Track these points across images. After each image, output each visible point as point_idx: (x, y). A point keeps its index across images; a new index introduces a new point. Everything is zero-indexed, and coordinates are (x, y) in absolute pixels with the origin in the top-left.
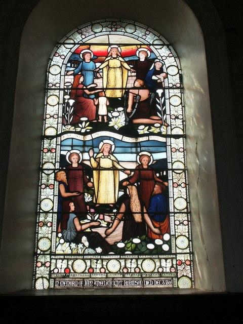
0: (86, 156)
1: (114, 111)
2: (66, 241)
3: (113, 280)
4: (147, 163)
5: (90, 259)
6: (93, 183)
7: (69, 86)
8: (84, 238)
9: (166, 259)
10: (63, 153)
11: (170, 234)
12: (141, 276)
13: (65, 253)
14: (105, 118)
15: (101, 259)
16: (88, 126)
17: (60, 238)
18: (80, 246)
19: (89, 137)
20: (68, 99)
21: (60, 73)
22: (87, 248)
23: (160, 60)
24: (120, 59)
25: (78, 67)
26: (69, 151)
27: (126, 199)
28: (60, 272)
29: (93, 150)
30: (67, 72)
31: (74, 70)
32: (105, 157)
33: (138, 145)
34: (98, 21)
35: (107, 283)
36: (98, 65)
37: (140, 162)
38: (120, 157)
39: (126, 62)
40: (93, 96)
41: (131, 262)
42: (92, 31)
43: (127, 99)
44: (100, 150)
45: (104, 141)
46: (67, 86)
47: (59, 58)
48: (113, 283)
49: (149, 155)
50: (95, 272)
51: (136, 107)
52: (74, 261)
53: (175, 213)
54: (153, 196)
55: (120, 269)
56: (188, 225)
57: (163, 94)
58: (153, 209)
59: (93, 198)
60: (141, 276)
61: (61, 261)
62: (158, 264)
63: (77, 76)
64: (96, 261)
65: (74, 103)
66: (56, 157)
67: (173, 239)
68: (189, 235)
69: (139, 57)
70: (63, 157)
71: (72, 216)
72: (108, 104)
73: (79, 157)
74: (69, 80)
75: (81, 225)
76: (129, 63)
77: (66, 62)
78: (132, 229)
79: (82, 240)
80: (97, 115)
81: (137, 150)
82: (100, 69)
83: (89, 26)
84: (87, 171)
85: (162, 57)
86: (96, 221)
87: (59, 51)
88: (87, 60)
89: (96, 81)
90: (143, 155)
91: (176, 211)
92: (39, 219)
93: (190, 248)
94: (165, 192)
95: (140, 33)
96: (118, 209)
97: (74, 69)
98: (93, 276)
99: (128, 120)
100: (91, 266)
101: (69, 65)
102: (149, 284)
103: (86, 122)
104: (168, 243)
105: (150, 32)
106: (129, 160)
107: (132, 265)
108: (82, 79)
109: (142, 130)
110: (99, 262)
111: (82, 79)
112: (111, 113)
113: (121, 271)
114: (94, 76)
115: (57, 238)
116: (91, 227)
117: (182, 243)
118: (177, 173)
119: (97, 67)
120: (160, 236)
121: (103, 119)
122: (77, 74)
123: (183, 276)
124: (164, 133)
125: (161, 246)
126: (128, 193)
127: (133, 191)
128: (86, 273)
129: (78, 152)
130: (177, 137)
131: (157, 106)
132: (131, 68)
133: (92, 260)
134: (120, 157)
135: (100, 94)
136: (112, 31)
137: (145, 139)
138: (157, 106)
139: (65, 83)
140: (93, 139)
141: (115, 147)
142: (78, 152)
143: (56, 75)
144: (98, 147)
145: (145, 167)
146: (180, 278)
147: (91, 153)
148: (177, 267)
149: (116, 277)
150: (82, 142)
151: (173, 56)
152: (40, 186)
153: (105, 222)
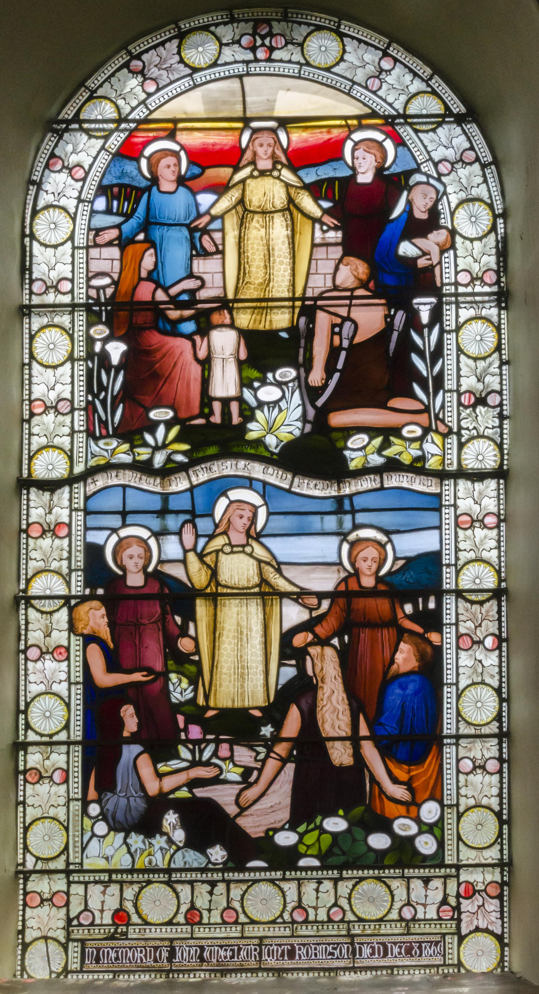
0: (172, 548)
1: (264, 382)
2: (114, 827)
3: (260, 945)
4: (374, 567)
5: (191, 883)
6: (196, 639)
7: (104, 288)
8: (171, 818)
9: (426, 881)
10: (96, 537)
11: (441, 802)
12: (349, 930)
13: (114, 865)
14: (234, 407)
15: (223, 881)
16: (177, 440)
17: (96, 819)
18: (159, 841)
19: (180, 484)
20: (105, 341)
21: (71, 238)
22: (179, 848)
23: (428, 176)
24: (287, 175)
25: (134, 210)
26: (114, 530)
27: (301, 691)
28: (98, 921)
29: (195, 526)
30: (96, 235)
31: (118, 226)
32: (233, 549)
33: (347, 507)
34: (204, 19)
35: (243, 953)
36: (205, 200)
37: (353, 564)
38: (284, 548)
39: (307, 187)
40: (189, 327)
41: (317, 890)
42: (182, 61)
43: (310, 334)
44: (217, 526)
45: (230, 493)
46: (98, 289)
47: (63, 176)
48: (260, 954)
49: (382, 538)
50: (205, 921)
51: (340, 366)
52: (141, 889)
53: (458, 737)
54: (390, 679)
55: (283, 911)
56: (500, 772)
57: (437, 315)
58: (390, 728)
59: (195, 690)
60: (349, 930)
61: (100, 888)
62: (400, 893)
63: (130, 249)
64: (209, 888)
65: (125, 356)
66: (70, 552)
67: (450, 817)
68: (501, 804)
69: (353, 168)
70: (94, 552)
71: (130, 751)
72: (243, 355)
73: (148, 549)
74: (104, 266)
75: (160, 776)
76: (315, 190)
77: (89, 191)
78: (322, 786)
79: (165, 824)
80: (206, 399)
81: (340, 523)
82: (214, 218)
83: (170, 40)
84: (175, 599)
85: (436, 165)
86: (208, 764)
87: (65, 148)
88: (167, 185)
89: (201, 266)
90: (359, 541)
91: (464, 730)
92: (25, 761)
93: (502, 844)
94: (431, 666)
95: (361, 59)
96: (278, 725)
97: (117, 220)
98: (200, 932)
99: (311, 413)
100: (192, 902)
101: (101, 204)
102: (373, 954)
103: (169, 424)
104: (435, 829)
105: (396, 60)
106: (314, 560)
107: (320, 895)
108: (148, 262)
109: (359, 451)
110: (217, 890)
111: (148, 262)
112: (256, 390)
113: (286, 916)
114: (193, 246)
115: (86, 819)
116: (193, 784)
117: (478, 832)
118: (472, 603)
119: (202, 209)
120: (412, 806)
121: (226, 413)
122: (131, 241)
123: (477, 929)
124: (433, 463)
125: (411, 839)
126: (310, 672)
127: (326, 665)
128: (178, 924)
129: (144, 534)
130: (478, 476)
131: (415, 358)
132: (326, 211)
133: (197, 885)
134: (284, 548)
135: (216, 318)
136: (256, 60)
137: (367, 483)
138: (415, 358)
139: (89, 279)
140: (191, 489)
141: (269, 514)
142: (144, 534)
143: (55, 247)
144: (211, 515)
145: (368, 582)
146: (466, 935)
147: (188, 537)
148: (459, 904)
149: (270, 934)
150: (158, 498)
151: (477, 159)
152: (24, 652)
153: (235, 765)
